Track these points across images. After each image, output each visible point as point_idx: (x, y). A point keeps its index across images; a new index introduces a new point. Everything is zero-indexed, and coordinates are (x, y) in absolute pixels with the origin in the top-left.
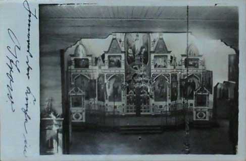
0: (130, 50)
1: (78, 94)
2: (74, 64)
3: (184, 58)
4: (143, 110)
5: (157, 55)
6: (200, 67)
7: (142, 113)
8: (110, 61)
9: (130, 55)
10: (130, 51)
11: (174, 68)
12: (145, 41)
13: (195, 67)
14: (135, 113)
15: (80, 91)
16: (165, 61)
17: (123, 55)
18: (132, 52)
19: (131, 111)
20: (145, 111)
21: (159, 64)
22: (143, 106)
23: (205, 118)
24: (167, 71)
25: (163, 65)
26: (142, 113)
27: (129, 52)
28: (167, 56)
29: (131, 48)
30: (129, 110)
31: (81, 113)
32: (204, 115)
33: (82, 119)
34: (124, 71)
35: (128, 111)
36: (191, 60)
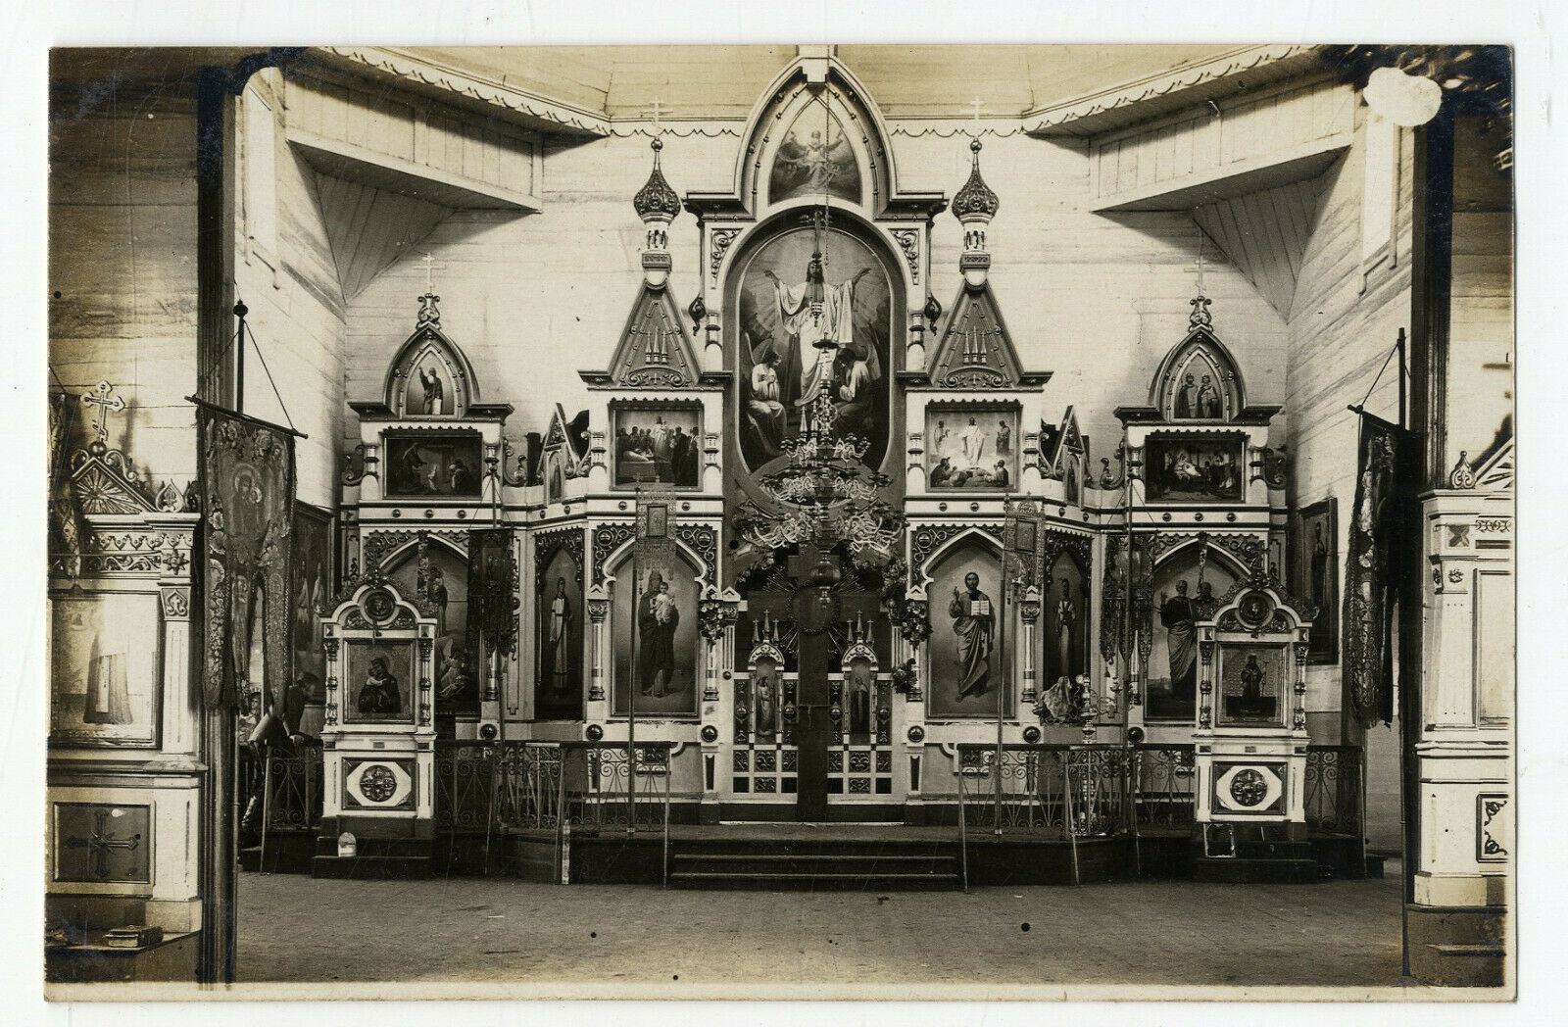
0: (759, 369)
1: (387, 635)
2: (380, 468)
3: (1137, 436)
4: (846, 775)
5: (948, 397)
6: (1256, 492)
7: (834, 799)
8: (625, 444)
9: (765, 407)
10: (763, 377)
11: (1072, 496)
12: (870, 314)
13: (1223, 498)
14: (790, 799)
15: (405, 613)
16: (1003, 444)
17: (713, 402)
18: (775, 388)
19: (766, 786)
20: (858, 787)
21: (960, 463)
22: (846, 747)
23: (411, 802)
24: (1241, 517)
25: (993, 473)
26: (834, 799)
27: (756, 385)
28: (1015, 408)
29: (769, 359)
30: (752, 774)
31: (409, 765)
32: (402, 778)
33: (411, 802)
34: (717, 507)
35: (741, 785)
36: (1192, 444)
